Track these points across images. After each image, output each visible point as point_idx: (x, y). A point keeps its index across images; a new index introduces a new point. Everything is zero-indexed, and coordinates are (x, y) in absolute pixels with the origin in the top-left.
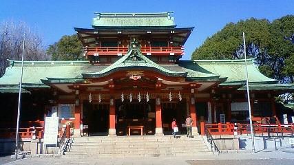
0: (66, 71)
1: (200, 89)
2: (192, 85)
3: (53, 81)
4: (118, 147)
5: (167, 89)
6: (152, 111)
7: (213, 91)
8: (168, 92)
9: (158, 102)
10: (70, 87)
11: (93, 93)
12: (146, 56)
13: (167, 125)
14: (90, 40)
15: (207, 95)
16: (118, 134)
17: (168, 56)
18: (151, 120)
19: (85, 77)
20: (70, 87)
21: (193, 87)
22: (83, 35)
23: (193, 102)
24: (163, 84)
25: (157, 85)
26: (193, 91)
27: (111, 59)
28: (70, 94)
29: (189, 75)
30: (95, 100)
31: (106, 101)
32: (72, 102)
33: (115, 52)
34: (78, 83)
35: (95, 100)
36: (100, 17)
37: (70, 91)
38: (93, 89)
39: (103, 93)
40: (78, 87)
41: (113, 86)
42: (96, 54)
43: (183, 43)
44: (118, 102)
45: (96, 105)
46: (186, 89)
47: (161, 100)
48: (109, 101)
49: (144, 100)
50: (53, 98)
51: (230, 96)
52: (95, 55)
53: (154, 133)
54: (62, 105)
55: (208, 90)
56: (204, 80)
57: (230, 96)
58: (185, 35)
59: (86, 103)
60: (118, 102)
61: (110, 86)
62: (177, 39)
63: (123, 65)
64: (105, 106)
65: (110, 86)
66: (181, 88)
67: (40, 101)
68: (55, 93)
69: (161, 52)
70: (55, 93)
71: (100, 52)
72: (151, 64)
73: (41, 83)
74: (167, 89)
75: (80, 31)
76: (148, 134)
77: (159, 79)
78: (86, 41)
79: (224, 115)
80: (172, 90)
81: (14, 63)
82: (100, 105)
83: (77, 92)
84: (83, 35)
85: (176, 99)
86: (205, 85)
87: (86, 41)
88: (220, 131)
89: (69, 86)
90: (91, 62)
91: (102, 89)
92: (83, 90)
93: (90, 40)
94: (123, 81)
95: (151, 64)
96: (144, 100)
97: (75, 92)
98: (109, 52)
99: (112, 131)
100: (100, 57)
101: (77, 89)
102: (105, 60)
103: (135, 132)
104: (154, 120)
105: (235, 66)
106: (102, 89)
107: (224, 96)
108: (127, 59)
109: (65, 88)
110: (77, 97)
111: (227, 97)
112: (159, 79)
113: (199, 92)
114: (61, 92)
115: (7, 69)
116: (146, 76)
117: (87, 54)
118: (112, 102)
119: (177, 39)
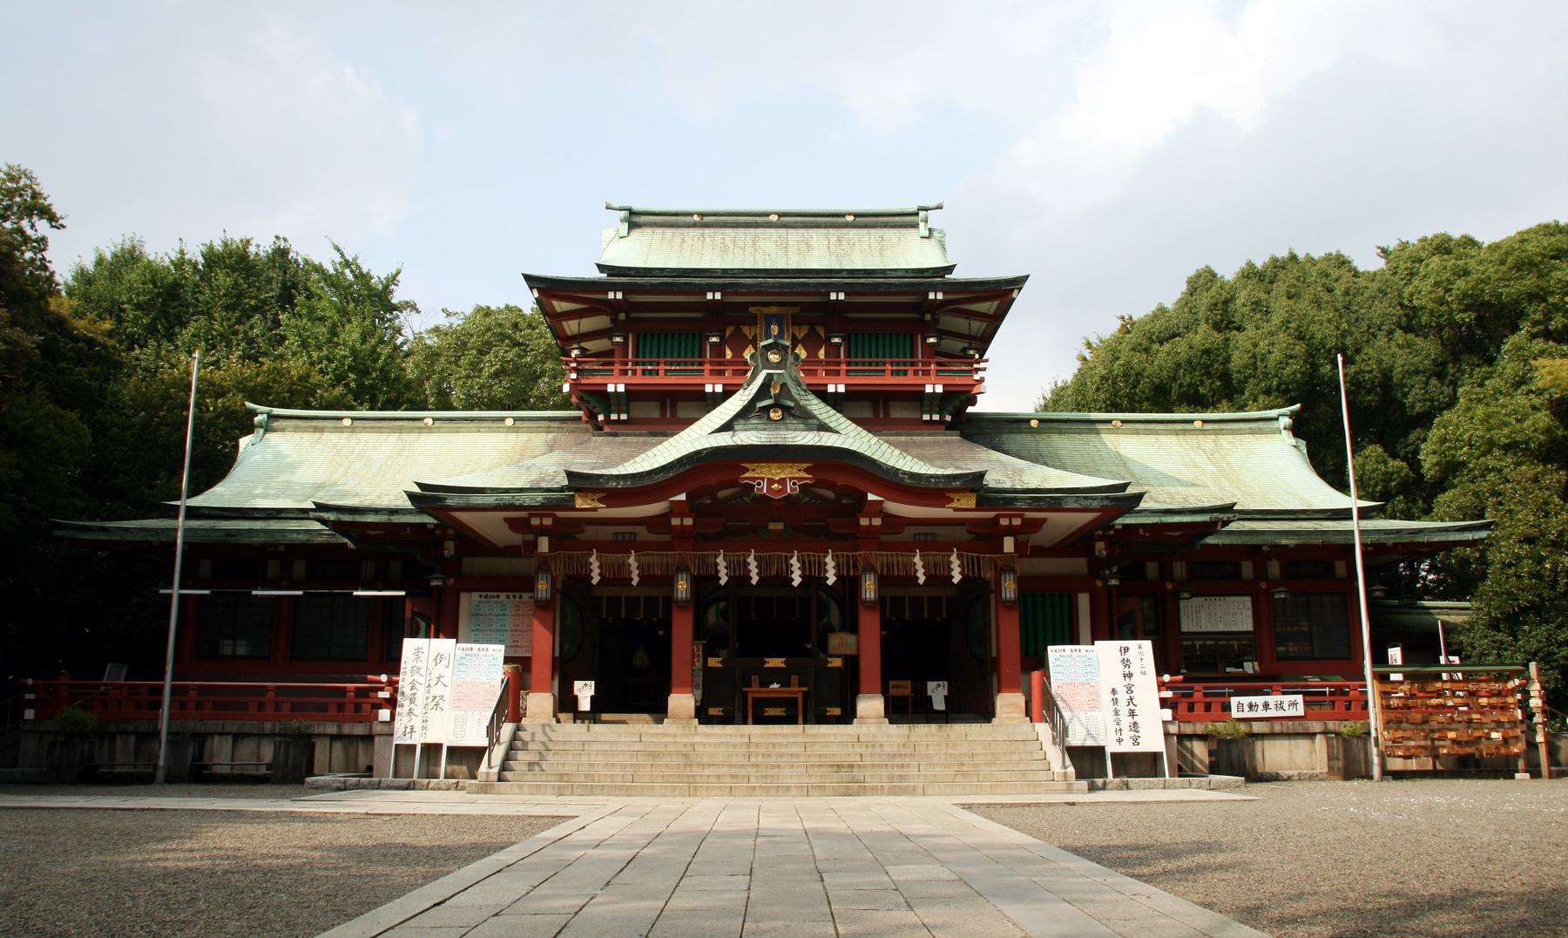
0: (493, 457)
1: (1036, 539)
2: (1004, 522)
3: (453, 500)
4: (706, 760)
5: (909, 532)
6: (843, 629)
7: (1100, 546)
8: (910, 548)
9: (869, 589)
10: (513, 524)
11: (603, 547)
12: (823, 395)
13: (904, 688)
14: (588, 324)
15: (1077, 565)
16: (702, 715)
17: (917, 397)
18: (837, 663)
19: (579, 482)
20: (513, 524)
21: (1010, 531)
22: (560, 306)
23: (1009, 589)
24: (889, 518)
25: (864, 522)
26: (1009, 545)
27: (676, 407)
28: (511, 551)
29: (994, 479)
30: (615, 577)
31: (659, 580)
32: (523, 584)
33: (698, 381)
34: (547, 508)
35: (615, 577)
36: (633, 226)
37: (516, 538)
38: (607, 533)
39: (640, 547)
40: (548, 521)
41: (688, 521)
42: (616, 387)
43: (984, 341)
44: (704, 583)
45: (614, 602)
46: (982, 537)
47: (882, 582)
48: (670, 582)
49: (813, 578)
50: (450, 566)
51: (1179, 569)
52: (611, 388)
53: (848, 716)
54: (475, 596)
55: (1078, 543)
56: (1052, 500)
57: (1179, 569)
58: (988, 307)
59: (573, 588)
60: (704, 583)
61: (675, 521)
62: (960, 324)
63: (725, 440)
64: (651, 602)
65: (675, 521)
66: (961, 533)
67: (427, 563)
68: (450, 548)
69: (886, 379)
70: (450, 548)
71: (630, 379)
72: (849, 436)
73: (408, 504)
74: (909, 532)
75: (547, 288)
76: (823, 719)
77: (871, 497)
78: (571, 327)
79: (1234, 701)
80: (931, 538)
81: (271, 417)
82: (633, 602)
83: (544, 544)
84: (560, 306)
85: (939, 578)
86: (1064, 522)
87: (571, 327)
88: (616, 372)
89: (506, 520)
90: (592, 416)
91: (643, 533)
92: (568, 534)
93: (588, 324)
94: (728, 498)
95: (849, 436)
96: (813, 578)
97: (535, 544)
98: (666, 377)
99: (682, 702)
100: (632, 395)
101: (542, 531)
102: (651, 411)
103: (771, 712)
104: (852, 662)
105: (1207, 442)
106: (643, 533)
107: (1152, 569)
108: (744, 414)
109: (491, 527)
110: (544, 565)
111: (1165, 573)
112: (871, 497)
113: (1039, 551)
114: (472, 543)
115: (244, 442)
116: (819, 483)
117: (575, 385)
118: (682, 587)
119: (960, 324)
